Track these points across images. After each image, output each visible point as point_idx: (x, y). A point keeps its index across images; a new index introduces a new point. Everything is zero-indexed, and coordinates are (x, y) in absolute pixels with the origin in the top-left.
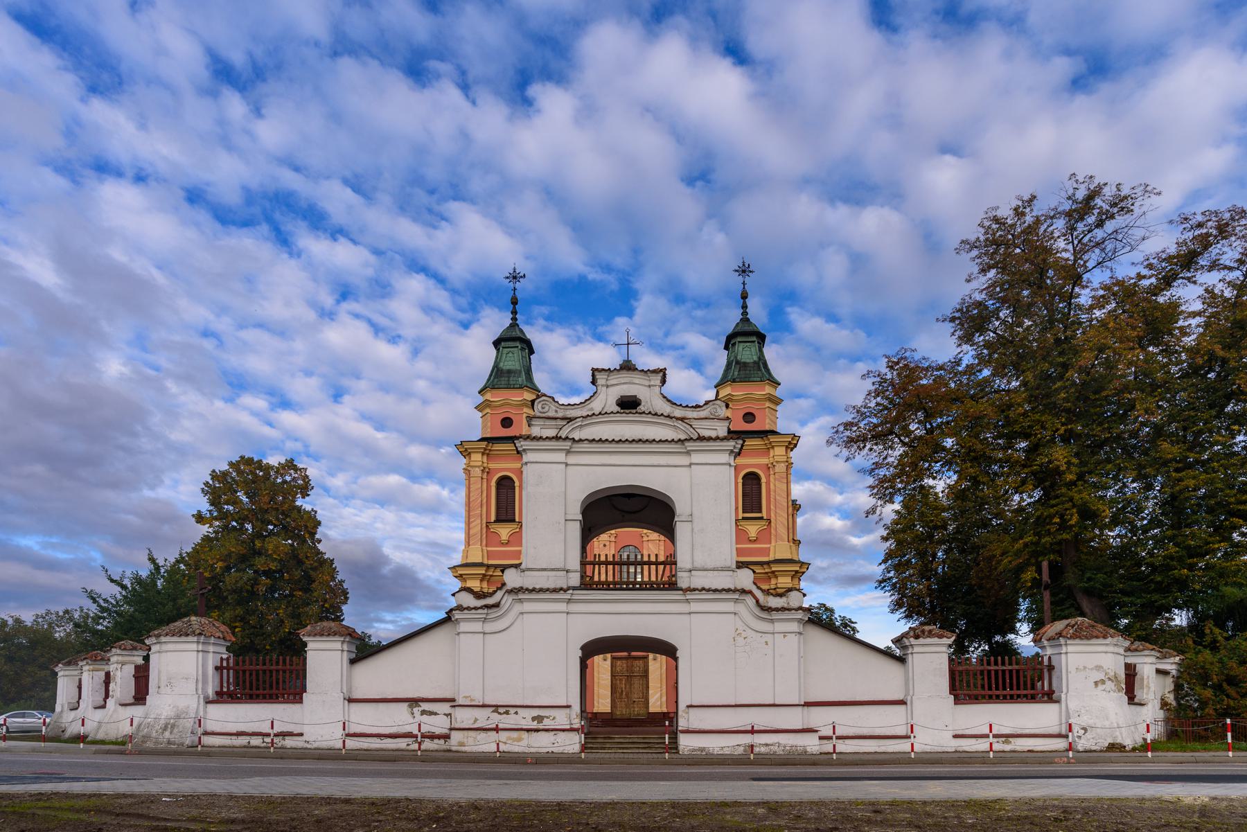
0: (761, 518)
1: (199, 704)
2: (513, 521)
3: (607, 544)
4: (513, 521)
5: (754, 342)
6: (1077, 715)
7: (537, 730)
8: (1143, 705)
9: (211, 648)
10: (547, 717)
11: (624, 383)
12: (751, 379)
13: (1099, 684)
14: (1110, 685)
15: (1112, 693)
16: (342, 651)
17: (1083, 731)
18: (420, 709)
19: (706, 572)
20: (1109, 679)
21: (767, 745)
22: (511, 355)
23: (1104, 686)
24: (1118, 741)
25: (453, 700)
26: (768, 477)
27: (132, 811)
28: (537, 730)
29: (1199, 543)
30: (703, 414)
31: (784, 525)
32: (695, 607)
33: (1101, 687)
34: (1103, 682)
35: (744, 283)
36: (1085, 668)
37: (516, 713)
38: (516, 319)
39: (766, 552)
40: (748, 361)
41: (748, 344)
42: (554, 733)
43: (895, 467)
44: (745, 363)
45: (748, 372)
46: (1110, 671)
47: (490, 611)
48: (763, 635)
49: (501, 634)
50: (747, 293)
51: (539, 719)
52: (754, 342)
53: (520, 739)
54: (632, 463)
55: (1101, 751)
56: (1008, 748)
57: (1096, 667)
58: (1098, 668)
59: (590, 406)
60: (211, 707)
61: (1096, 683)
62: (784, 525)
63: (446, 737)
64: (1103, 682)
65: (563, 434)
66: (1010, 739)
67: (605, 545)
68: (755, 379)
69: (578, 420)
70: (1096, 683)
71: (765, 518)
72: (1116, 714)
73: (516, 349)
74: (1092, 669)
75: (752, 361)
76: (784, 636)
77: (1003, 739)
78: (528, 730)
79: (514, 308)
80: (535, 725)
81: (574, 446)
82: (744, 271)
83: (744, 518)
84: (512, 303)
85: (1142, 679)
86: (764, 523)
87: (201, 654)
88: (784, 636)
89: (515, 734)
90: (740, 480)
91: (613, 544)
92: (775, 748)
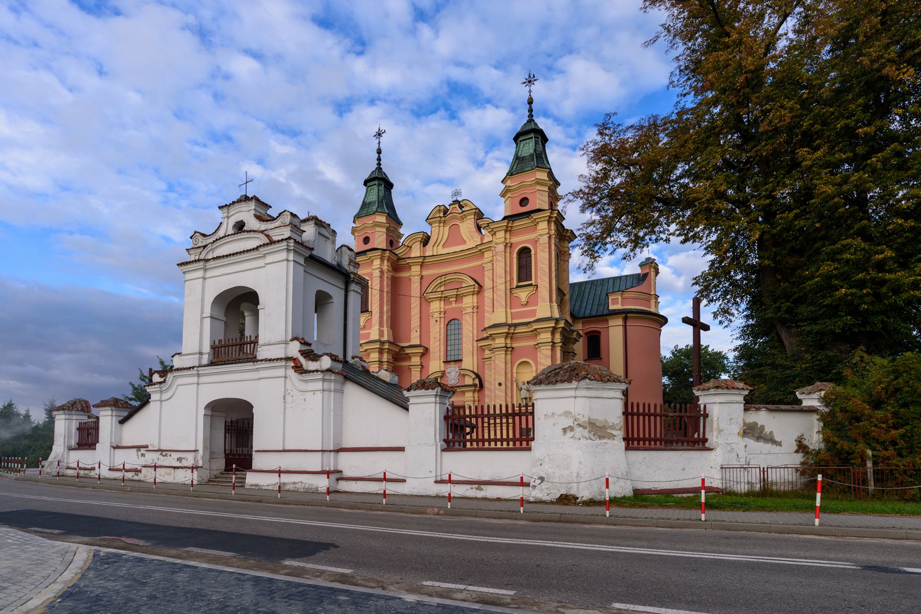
0: (531, 285)
1: (64, 449)
2: (368, 311)
3: (438, 319)
4: (368, 311)
5: (532, 138)
6: (539, 463)
7: (178, 468)
8: (712, 450)
9: (75, 417)
10: (184, 458)
11: (237, 212)
12: (525, 170)
13: (568, 432)
14: (579, 431)
15: (583, 441)
16: (436, 403)
17: (540, 481)
18: (141, 452)
19: (269, 346)
20: (579, 425)
21: (294, 483)
22: (372, 191)
23: (573, 433)
24: (572, 492)
25: (147, 447)
26: (536, 249)
27: (778, 501)
28: (178, 468)
29: (859, 256)
30: (277, 223)
31: (546, 288)
32: (263, 374)
33: (569, 434)
34: (571, 429)
35: (530, 91)
36: (553, 414)
37: (170, 455)
38: (380, 164)
39: (533, 312)
40: (526, 155)
41: (527, 141)
42: (185, 470)
43: (601, 223)
44: (523, 157)
45: (523, 164)
46: (580, 417)
47: (162, 386)
48: (303, 393)
49: (169, 401)
50: (532, 99)
51: (180, 459)
52: (532, 138)
53: (170, 474)
54: (246, 268)
55: (552, 503)
56: (480, 494)
57: (565, 413)
58: (567, 414)
59: (218, 234)
60: (72, 452)
61: (565, 430)
62: (546, 288)
63: (137, 471)
64: (571, 429)
65: (202, 257)
66: (482, 487)
67: (436, 321)
68: (527, 169)
69: (209, 245)
70: (565, 430)
71: (534, 284)
72: (580, 463)
73: (375, 186)
74: (560, 415)
75: (529, 154)
76: (314, 394)
77: (476, 486)
78: (174, 468)
79: (379, 156)
80: (178, 464)
81: (207, 264)
82: (530, 82)
83: (518, 287)
84: (378, 153)
85: (712, 421)
86: (531, 288)
87: (67, 421)
88: (314, 394)
89: (168, 470)
90: (515, 256)
91: (442, 319)
92: (298, 486)
